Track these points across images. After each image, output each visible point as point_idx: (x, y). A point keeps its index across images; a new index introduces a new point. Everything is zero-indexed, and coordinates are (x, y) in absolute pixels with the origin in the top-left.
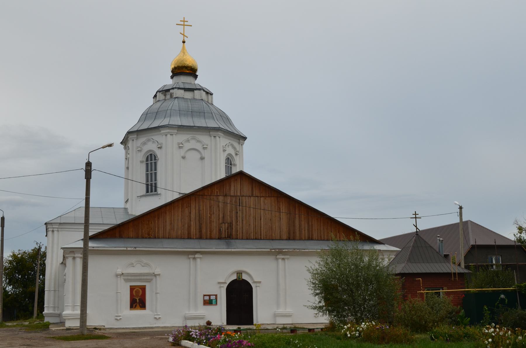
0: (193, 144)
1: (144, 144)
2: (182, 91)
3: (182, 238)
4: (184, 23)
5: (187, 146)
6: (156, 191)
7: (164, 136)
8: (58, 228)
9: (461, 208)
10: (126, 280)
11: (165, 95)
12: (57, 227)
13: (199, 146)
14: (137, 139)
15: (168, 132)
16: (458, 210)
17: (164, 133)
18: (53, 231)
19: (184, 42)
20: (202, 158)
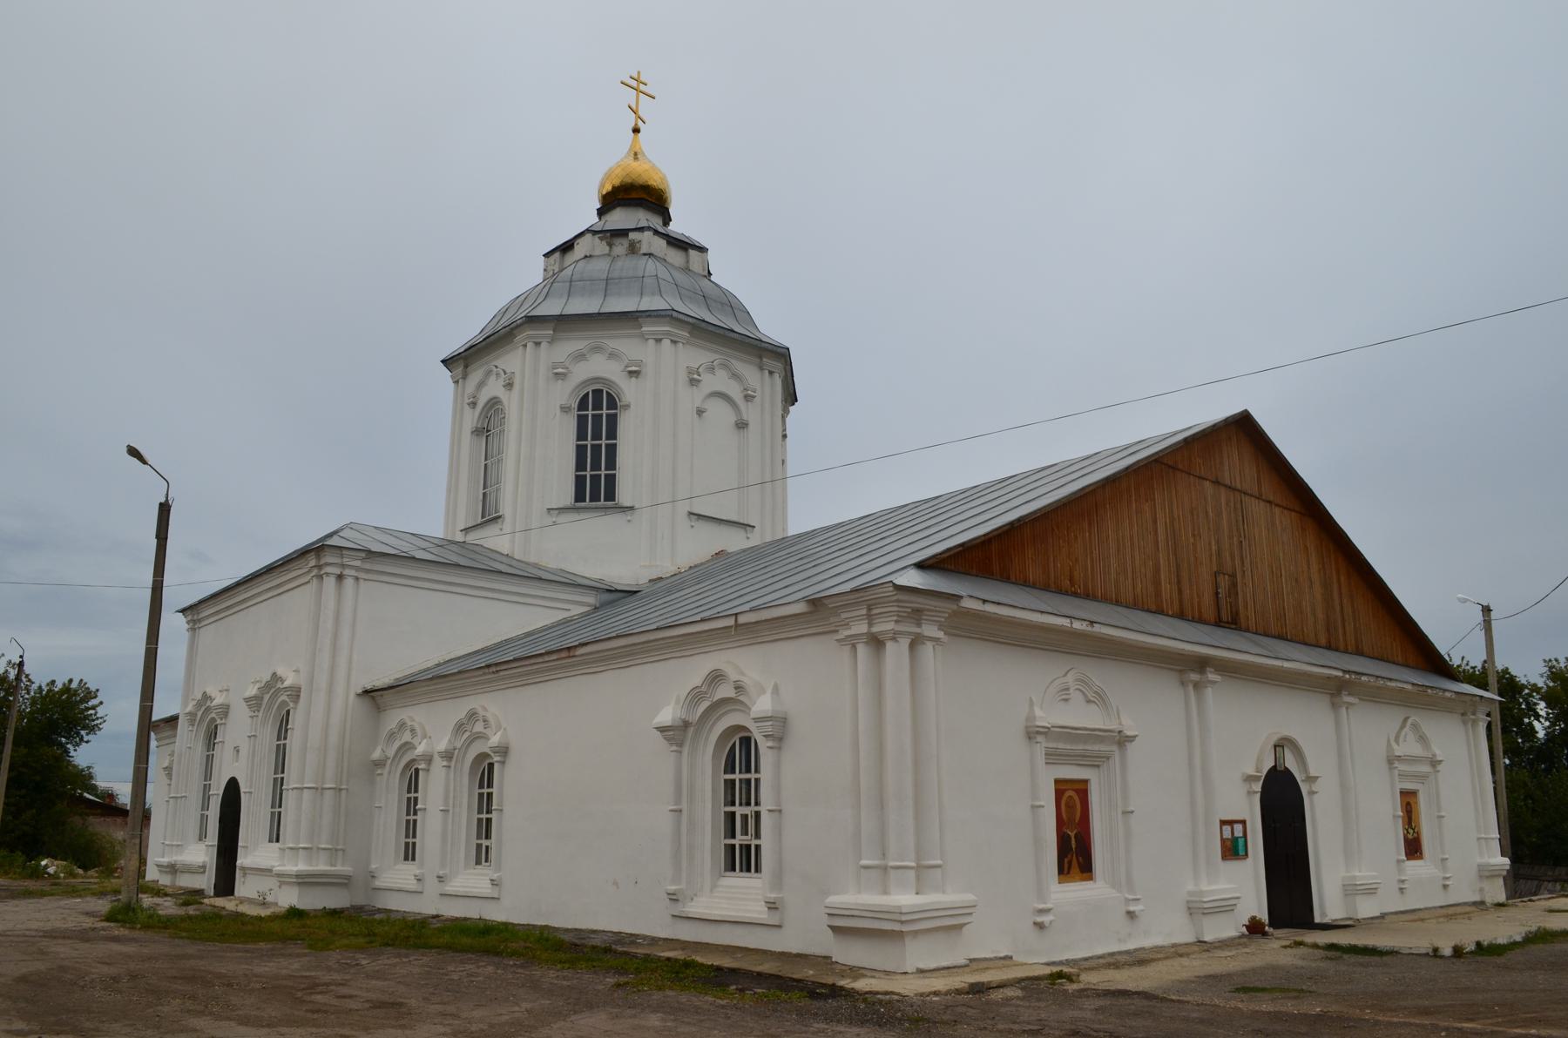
0: (719, 381)
1: (580, 357)
2: (663, 243)
3: (1136, 605)
4: (637, 84)
5: (711, 382)
6: (611, 496)
7: (651, 342)
8: (357, 569)
9: (1487, 610)
10: (1053, 757)
11: (610, 245)
12: (358, 563)
13: (735, 391)
14: (552, 341)
15: (668, 333)
16: (1479, 617)
17: (654, 333)
18: (340, 577)
19: (636, 131)
20: (742, 425)
